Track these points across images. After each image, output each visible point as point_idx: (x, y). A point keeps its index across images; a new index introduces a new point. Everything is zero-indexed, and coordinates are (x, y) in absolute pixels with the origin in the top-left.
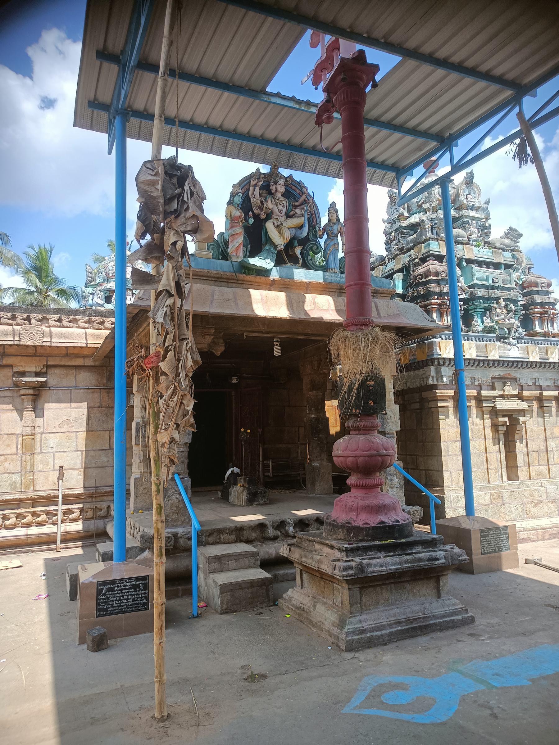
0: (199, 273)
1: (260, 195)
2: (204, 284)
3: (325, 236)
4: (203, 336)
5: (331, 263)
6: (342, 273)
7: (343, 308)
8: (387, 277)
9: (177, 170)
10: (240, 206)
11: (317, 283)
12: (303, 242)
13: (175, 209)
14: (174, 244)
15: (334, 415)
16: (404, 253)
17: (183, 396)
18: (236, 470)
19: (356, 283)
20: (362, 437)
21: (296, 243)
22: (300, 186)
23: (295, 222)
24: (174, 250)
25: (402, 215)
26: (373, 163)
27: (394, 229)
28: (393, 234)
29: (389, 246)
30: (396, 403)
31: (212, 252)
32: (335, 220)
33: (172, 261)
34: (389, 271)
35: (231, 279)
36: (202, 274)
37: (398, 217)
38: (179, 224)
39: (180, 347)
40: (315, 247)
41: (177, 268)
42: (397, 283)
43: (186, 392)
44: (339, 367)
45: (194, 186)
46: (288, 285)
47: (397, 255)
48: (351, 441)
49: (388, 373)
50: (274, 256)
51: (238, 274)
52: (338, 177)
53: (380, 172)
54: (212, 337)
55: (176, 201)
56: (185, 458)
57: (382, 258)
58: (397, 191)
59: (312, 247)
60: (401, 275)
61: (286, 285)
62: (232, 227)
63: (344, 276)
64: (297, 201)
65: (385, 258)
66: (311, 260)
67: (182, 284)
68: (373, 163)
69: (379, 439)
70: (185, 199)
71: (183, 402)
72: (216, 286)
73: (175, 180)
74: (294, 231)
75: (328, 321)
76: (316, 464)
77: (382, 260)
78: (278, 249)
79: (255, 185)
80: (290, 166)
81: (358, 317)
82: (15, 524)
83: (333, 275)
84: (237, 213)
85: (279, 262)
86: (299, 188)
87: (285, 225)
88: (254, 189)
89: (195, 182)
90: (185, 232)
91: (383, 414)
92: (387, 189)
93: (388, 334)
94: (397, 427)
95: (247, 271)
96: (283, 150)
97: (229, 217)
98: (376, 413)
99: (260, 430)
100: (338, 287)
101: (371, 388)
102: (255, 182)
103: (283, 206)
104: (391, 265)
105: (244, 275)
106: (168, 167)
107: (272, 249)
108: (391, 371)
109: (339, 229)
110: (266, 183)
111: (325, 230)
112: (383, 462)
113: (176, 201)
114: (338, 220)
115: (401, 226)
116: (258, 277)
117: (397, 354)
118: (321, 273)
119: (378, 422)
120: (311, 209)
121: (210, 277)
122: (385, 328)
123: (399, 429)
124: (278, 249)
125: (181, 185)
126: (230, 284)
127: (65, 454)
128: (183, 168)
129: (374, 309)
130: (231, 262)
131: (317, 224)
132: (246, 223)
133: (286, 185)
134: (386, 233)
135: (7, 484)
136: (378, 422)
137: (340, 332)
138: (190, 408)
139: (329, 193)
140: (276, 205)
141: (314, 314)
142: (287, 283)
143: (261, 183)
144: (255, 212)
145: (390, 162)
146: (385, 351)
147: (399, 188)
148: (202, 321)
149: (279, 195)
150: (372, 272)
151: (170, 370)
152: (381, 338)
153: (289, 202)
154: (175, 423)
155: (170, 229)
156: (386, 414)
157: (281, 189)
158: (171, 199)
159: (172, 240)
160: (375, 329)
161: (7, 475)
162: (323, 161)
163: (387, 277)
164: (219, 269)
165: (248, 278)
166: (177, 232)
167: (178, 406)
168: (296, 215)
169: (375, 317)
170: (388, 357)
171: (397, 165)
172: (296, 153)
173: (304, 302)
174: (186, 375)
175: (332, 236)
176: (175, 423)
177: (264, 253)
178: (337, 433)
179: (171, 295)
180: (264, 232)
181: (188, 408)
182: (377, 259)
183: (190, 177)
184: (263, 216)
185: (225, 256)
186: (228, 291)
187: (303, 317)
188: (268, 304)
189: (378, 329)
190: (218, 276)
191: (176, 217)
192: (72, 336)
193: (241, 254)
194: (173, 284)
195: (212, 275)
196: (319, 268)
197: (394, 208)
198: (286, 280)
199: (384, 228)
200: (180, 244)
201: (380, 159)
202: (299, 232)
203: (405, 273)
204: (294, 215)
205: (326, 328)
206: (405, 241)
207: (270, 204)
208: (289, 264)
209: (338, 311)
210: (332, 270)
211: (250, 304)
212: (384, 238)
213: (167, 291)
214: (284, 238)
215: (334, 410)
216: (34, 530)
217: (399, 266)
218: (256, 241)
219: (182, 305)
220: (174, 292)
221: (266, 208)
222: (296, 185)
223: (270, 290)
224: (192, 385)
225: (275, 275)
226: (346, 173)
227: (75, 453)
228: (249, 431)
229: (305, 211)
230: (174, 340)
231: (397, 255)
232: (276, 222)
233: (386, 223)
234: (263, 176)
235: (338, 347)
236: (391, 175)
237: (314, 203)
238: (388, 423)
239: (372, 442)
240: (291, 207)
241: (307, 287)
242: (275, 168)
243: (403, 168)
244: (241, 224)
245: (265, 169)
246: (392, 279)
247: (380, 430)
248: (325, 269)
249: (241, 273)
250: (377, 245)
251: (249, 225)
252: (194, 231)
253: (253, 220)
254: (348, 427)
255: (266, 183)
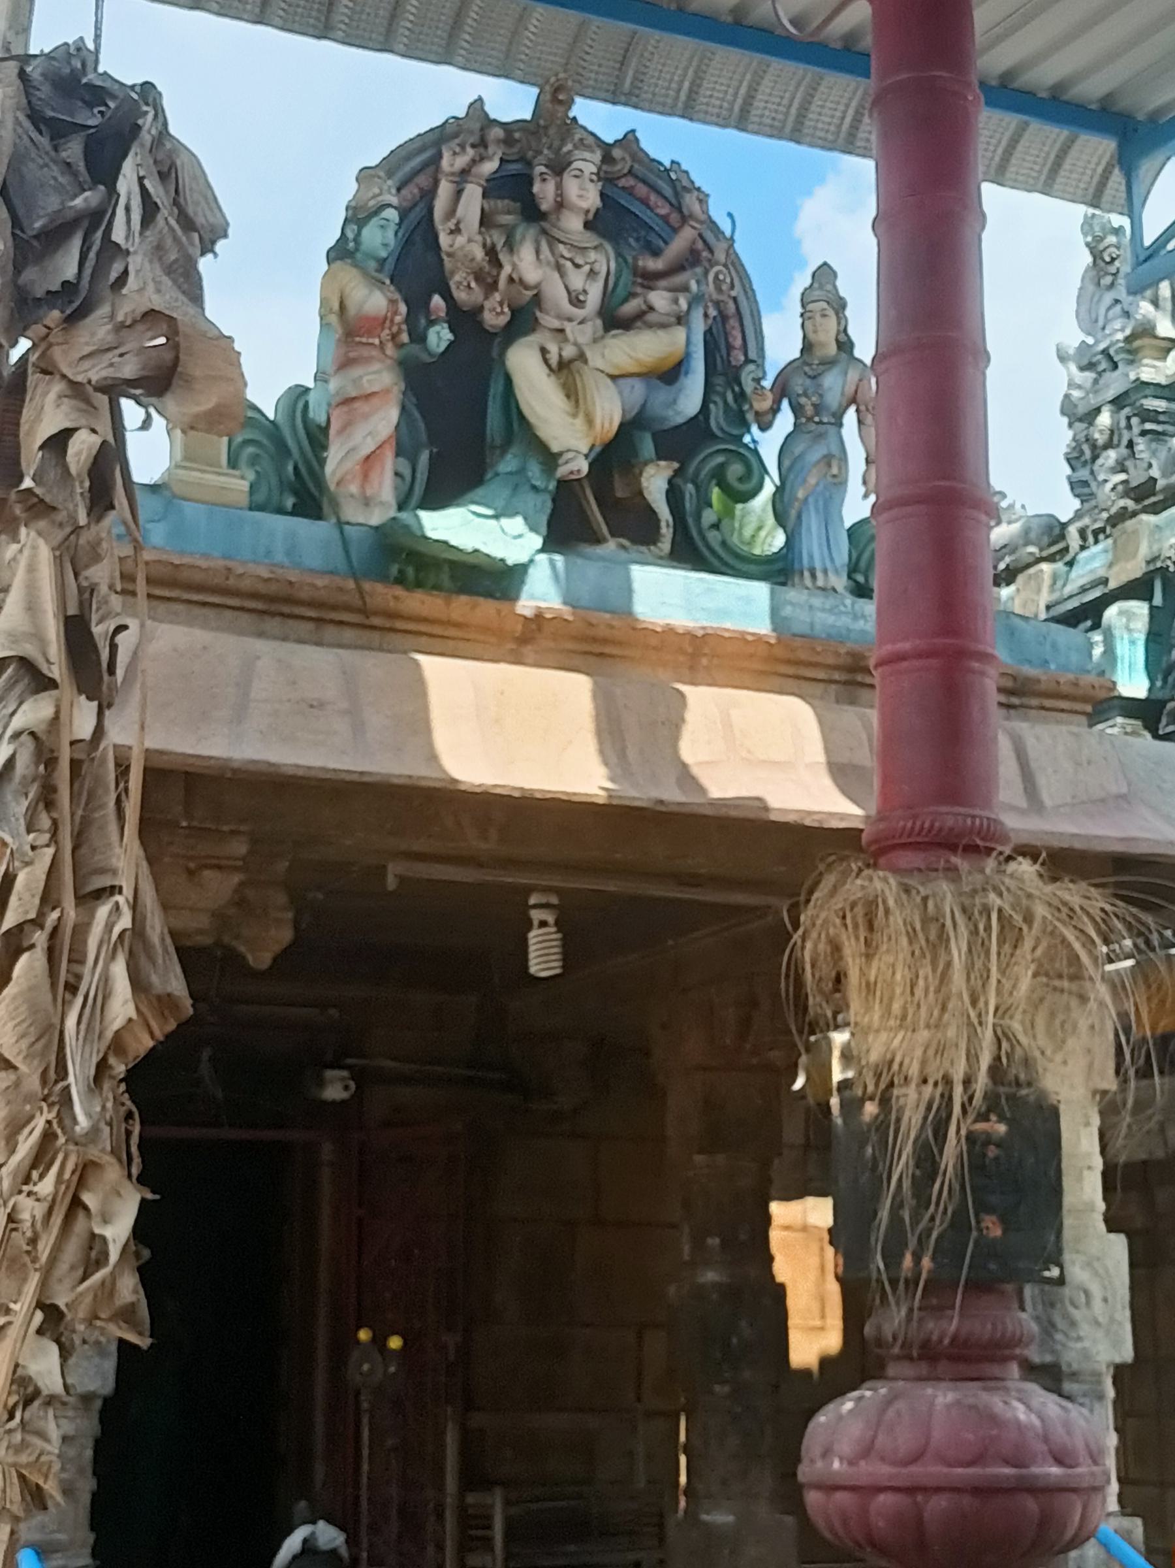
0: (185, 575)
1: (486, 221)
2: (205, 626)
3: (785, 421)
4: (191, 873)
5: (812, 547)
6: (862, 591)
7: (866, 757)
8: (1071, 619)
9: (90, 105)
10: (390, 265)
11: (741, 638)
12: (682, 442)
13: (65, 284)
14: (59, 442)
15: (813, 1275)
16: (1156, 509)
17: (86, 1172)
18: (328, 1535)
19: (930, 653)
20: (943, 1396)
21: (647, 447)
22: (674, 189)
23: (644, 348)
24: (52, 474)
25: (1146, 330)
26: (1010, 94)
27: (1111, 394)
28: (1105, 419)
29: (1083, 474)
30: (1113, 1224)
31: (251, 476)
32: (832, 349)
33: (42, 524)
34: (1084, 590)
35: (334, 608)
36: (198, 577)
37: (1127, 340)
38: (90, 349)
39: (81, 931)
40: (735, 470)
41: (73, 558)
42: (1122, 648)
43: (93, 1153)
44: (839, 1038)
45: (163, 176)
46: (605, 641)
47: (1123, 515)
48: (891, 1413)
49: (1076, 1081)
50: (546, 504)
51: (367, 586)
52: (849, 146)
53: (1043, 136)
54: (236, 878)
55: (76, 243)
56: (81, 1471)
57: (1050, 528)
58: (1125, 222)
59: (722, 467)
60: (1140, 609)
61: (595, 642)
62: (345, 364)
63: (869, 608)
64: (656, 253)
65: (1064, 526)
66: (716, 526)
67: (98, 630)
68: (1010, 94)
69: (1026, 1407)
70: (118, 235)
71: (88, 1198)
72: (261, 635)
73: (74, 150)
74: (637, 391)
75: (790, 818)
76: (720, 1518)
77: (1053, 538)
78: (561, 471)
79: (465, 173)
80: (630, 94)
81: (933, 813)
83: (817, 601)
84: (374, 300)
85: (565, 531)
86: (668, 191)
87: (595, 359)
88: (459, 193)
89: (170, 165)
90: (113, 390)
91: (1049, 1281)
92: (1080, 211)
93: (1072, 893)
94: (1116, 1344)
95: (410, 572)
96: (596, 21)
97: (333, 319)
98: (1019, 1278)
99: (451, 1340)
100: (841, 661)
101: (992, 1152)
102: (461, 162)
103: (592, 274)
104: (1094, 563)
105: (399, 591)
106: (45, 91)
107: (535, 471)
108: (1090, 1066)
109: (850, 389)
110: (520, 169)
111: (782, 389)
112: (1048, 1522)
113: (76, 243)
114: (845, 345)
115: (1141, 385)
116: (464, 598)
117: (1116, 986)
118: (760, 591)
119: (1027, 1321)
120: (719, 289)
121: (236, 593)
122: (1062, 862)
123: (1127, 1353)
124: (561, 471)
125: (103, 171)
126: (330, 632)
128: (114, 97)
129: (1007, 769)
130: (340, 524)
131: (748, 361)
132: (415, 349)
133: (606, 179)
134: (1068, 408)
136: (1027, 1321)
137: (845, 875)
138: (118, 1231)
139: (808, 220)
140: (559, 268)
141: (724, 783)
142: (602, 632)
143: (489, 167)
144: (460, 295)
145: (1092, 89)
146: (1062, 973)
147: (1132, 209)
148: (186, 802)
149: (573, 223)
150: (1005, 592)
151: (24, 1044)
152: (1040, 911)
153: (619, 255)
154: (40, 1305)
155: (45, 372)
156: (1061, 1281)
157: (583, 193)
158: (55, 236)
159: (49, 427)
160: (1012, 867)
162: (782, 78)
163: (1071, 619)
164: (279, 557)
165: (416, 602)
166: (76, 390)
167: (57, 1220)
168: (651, 317)
169: (1013, 808)
170: (1074, 1002)
171: (1123, 104)
172: (657, 34)
173: (674, 724)
174: (102, 1067)
175: (816, 421)
176: (40, 1305)
177: (495, 489)
178: (826, 1362)
179: (42, 683)
180: (496, 388)
181: (108, 1232)
182: (1026, 531)
183: (146, 137)
184: (495, 318)
185: (308, 497)
186: (318, 664)
187: (672, 794)
188: (505, 730)
189: (1025, 868)
190: (273, 588)
191: (73, 319)
193: (386, 488)
194: (52, 629)
195: (246, 584)
196: (753, 568)
197: (1108, 298)
198: (595, 617)
199: (1064, 389)
200: (82, 447)
201: (1045, 75)
202: (662, 394)
203: (1158, 600)
204: (640, 316)
205: (778, 855)
206: (1163, 454)
207: (527, 263)
208: (611, 545)
209: (842, 773)
210: (813, 576)
211: (417, 723)
212: (1063, 436)
213: (24, 662)
214: (590, 422)
215: (815, 1247)
217: (1134, 569)
218: (460, 427)
219: (99, 731)
220: (57, 669)
221: (511, 280)
222: (652, 178)
223: (517, 659)
224: (129, 1116)
225: (542, 591)
226: (885, 136)
228: (395, 1343)
229: (694, 301)
230: (49, 899)
231: (1123, 515)
232: (553, 349)
233: (1073, 368)
234: (497, 133)
235: (836, 948)
236: (1097, 148)
237: (735, 264)
238: (1073, 1324)
239: (993, 1419)
240: (626, 276)
241: (695, 656)
242: (555, 99)
243: (1153, 117)
244: (390, 349)
245: (512, 101)
246: (1097, 625)
247: (1036, 1358)
248: (779, 570)
249: (383, 578)
250: (1026, 464)
251: (427, 359)
252: (158, 383)
253: (447, 335)
254: (879, 1342)
255: (514, 168)
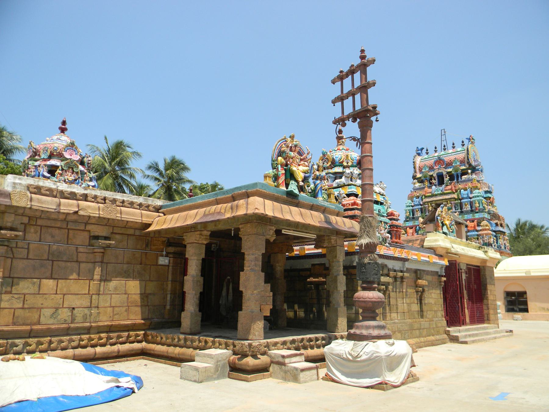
82: (68, 346)
127: (118, 296)
135: (81, 315)
161: (81, 309)
192: (133, 214)
216: (99, 349)
227: (124, 295)
